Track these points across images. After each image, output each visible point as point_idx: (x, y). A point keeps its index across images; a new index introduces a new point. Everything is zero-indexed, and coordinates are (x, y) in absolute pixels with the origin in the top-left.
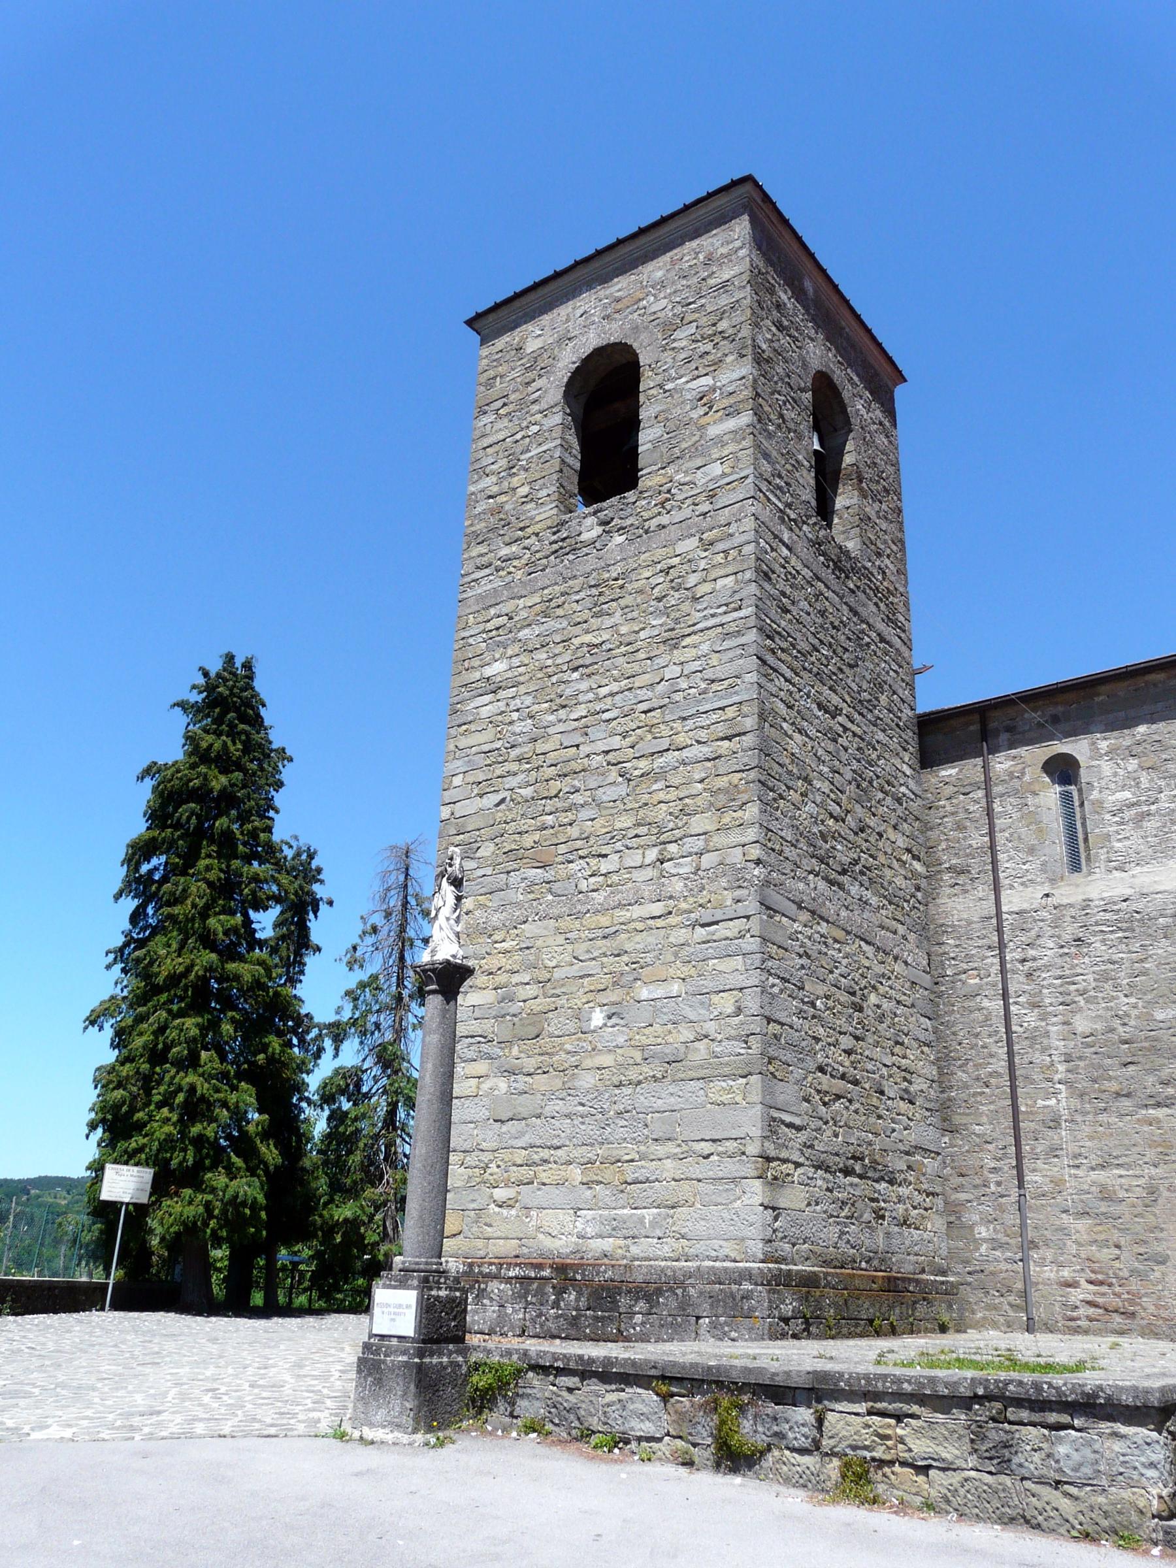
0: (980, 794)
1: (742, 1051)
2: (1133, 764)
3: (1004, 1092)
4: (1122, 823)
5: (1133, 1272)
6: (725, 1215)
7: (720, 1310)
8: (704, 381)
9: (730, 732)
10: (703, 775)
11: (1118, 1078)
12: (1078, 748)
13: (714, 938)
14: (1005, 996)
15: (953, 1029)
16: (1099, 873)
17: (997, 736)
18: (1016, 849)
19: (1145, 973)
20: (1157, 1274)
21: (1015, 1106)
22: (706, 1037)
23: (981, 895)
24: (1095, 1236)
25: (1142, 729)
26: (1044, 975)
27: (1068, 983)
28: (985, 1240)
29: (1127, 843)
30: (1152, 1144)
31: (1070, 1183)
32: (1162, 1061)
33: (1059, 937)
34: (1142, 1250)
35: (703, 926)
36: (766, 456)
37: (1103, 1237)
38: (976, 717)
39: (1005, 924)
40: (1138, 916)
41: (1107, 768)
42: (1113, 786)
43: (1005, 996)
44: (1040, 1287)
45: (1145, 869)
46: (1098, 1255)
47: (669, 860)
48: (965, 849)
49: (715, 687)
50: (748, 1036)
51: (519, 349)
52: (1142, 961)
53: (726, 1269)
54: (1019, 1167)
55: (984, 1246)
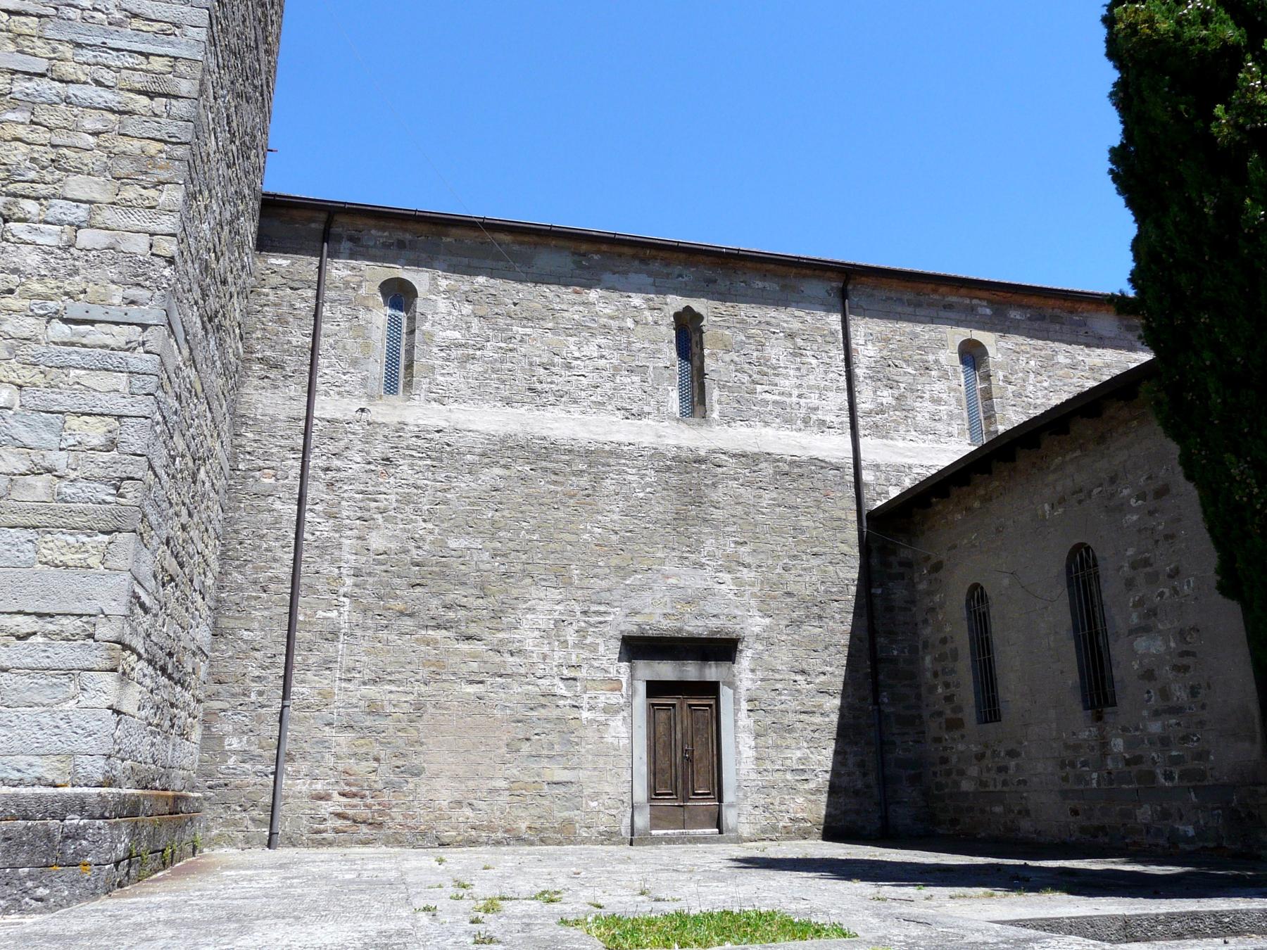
0: (311, 293)
1: (109, 499)
2: (467, 309)
3: (283, 599)
4: (448, 360)
5: (388, 784)
6: (46, 720)
7: (22, 858)
9: (154, 87)
10: (99, 127)
11: (407, 596)
12: (419, 278)
13: (84, 341)
14: (301, 501)
15: (236, 527)
16: (418, 400)
17: (339, 242)
18: (339, 357)
19: (446, 502)
20: (411, 786)
21: (292, 614)
22: (49, 471)
23: (292, 394)
24: (356, 750)
25: (481, 279)
26: (345, 487)
27: (369, 499)
28: (235, 752)
29: (450, 379)
30: (426, 663)
31: (339, 698)
32: (448, 586)
33: (368, 453)
34: (400, 763)
35: (67, 321)
37: (364, 750)
38: (323, 216)
39: (314, 428)
40: (448, 449)
41: (442, 305)
42: (445, 323)
43: (301, 501)
44: (289, 800)
45: (462, 407)
46: (355, 768)
47: (19, 220)
48: (282, 344)
49: (136, 23)
50: (122, 480)
52: (445, 490)
53: (39, 798)
54: (286, 679)
55: (234, 758)
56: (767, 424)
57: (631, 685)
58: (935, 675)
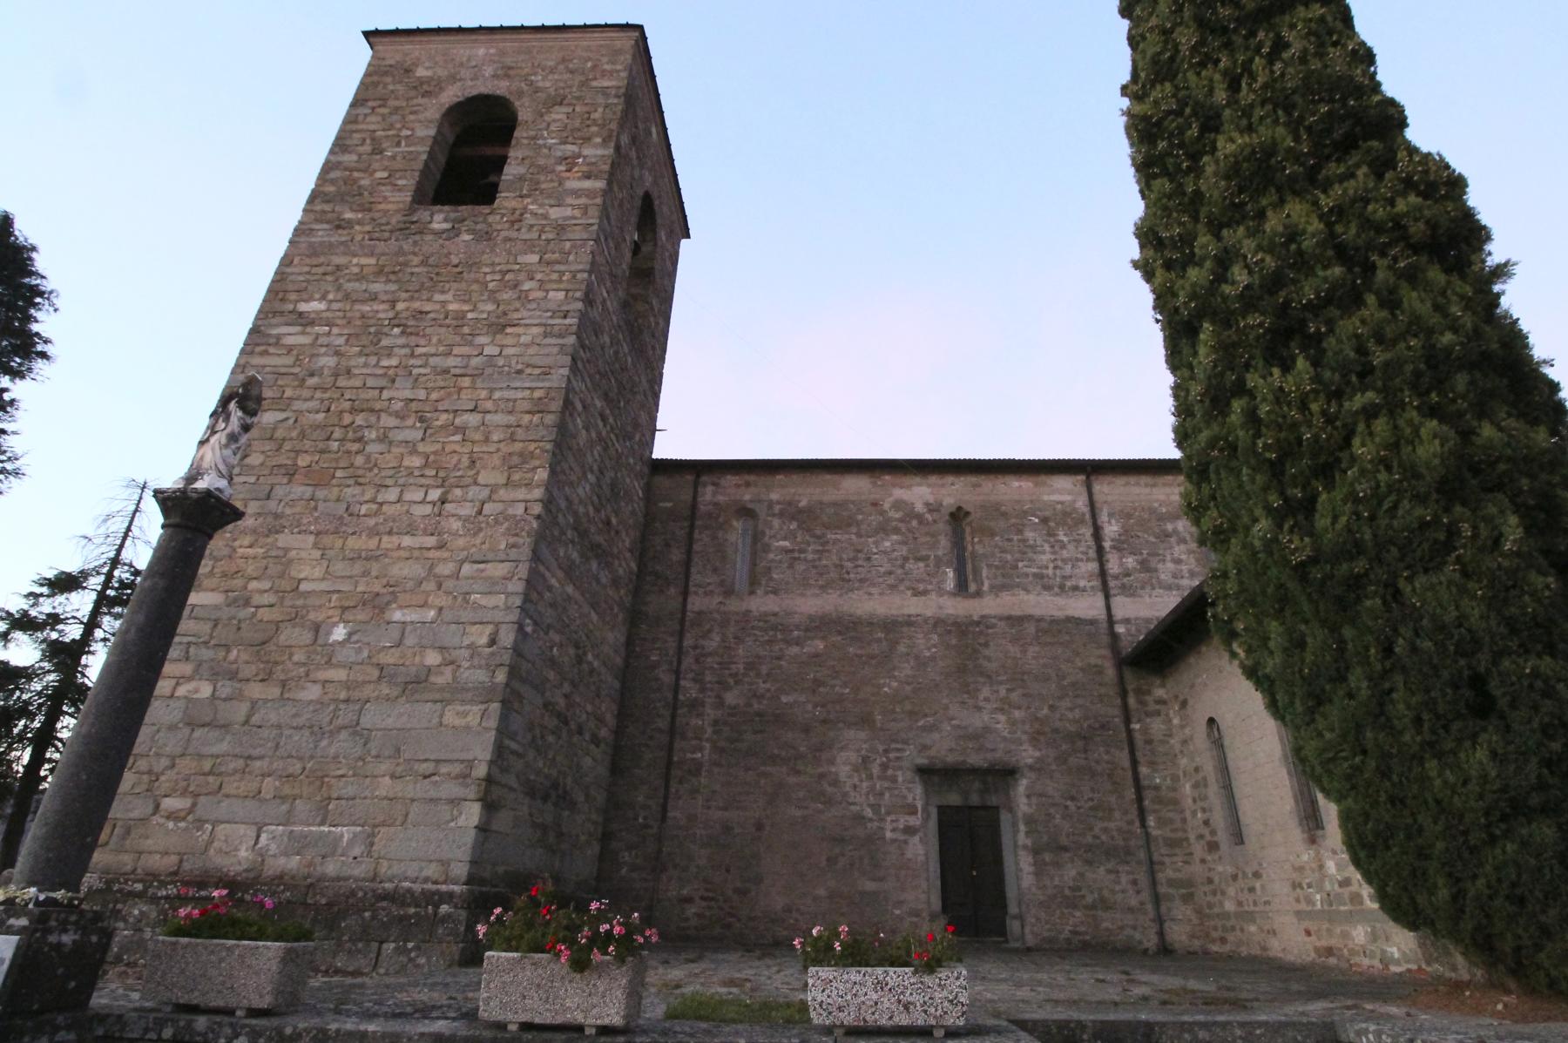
8: (569, 147)
36: (608, 218)
49: (529, 371)
51: (407, 71)
56: (1028, 591)
57: (925, 810)
58: (1194, 801)
